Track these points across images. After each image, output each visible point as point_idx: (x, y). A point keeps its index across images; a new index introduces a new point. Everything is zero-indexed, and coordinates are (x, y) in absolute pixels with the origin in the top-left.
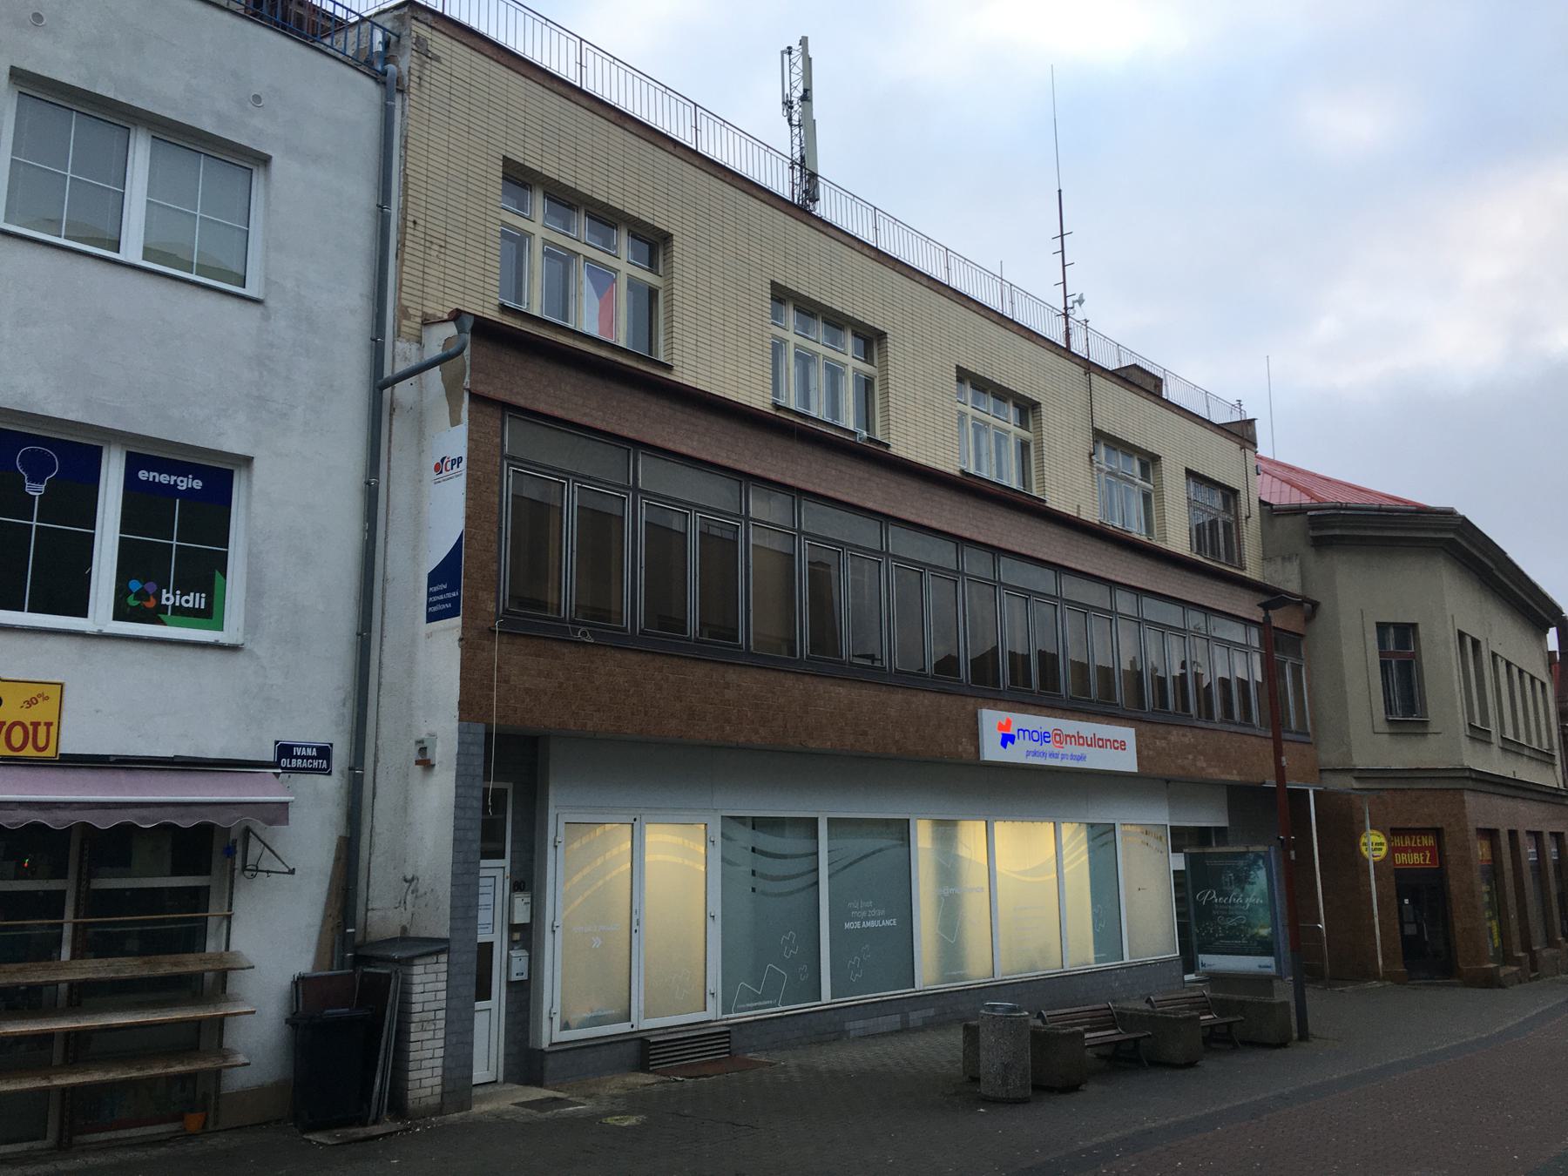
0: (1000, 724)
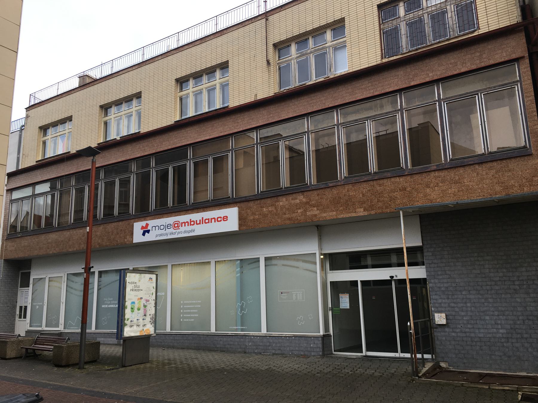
0: (142, 226)
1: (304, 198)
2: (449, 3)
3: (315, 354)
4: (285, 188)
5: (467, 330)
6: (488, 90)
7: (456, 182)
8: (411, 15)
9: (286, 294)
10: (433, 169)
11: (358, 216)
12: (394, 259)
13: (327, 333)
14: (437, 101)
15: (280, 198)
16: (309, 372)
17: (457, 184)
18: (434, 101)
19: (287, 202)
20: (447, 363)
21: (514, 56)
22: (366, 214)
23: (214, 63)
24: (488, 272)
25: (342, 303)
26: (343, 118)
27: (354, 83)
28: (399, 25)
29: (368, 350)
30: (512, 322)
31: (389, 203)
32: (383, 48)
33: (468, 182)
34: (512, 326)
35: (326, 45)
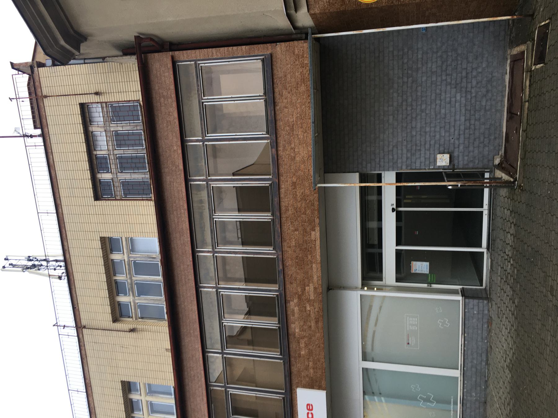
1: (293, 301)
2: (108, 128)
3: (487, 310)
4: (279, 323)
5: (457, 132)
6: (200, 93)
7: (292, 129)
8: (113, 166)
9: (410, 339)
10: (276, 152)
11: (320, 238)
12: (373, 198)
13: (460, 293)
14: (203, 144)
15: (291, 331)
16: (513, 314)
17: (295, 128)
18: (204, 146)
19: (297, 323)
20: (495, 157)
21: (170, 65)
22: (319, 228)
23: (121, 400)
24: (392, 107)
25: (422, 271)
26: (207, 246)
27: (171, 230)
28: (120, 180)
29: (480, 246)
30: (449, 87)
31: (308, 201)
32: (141, 198)
33: (293, 118)
34: (453, 86)
35: (126, 260)
